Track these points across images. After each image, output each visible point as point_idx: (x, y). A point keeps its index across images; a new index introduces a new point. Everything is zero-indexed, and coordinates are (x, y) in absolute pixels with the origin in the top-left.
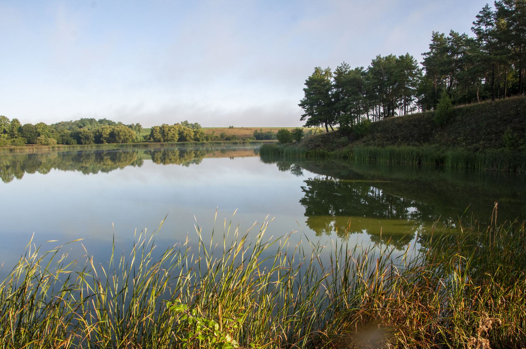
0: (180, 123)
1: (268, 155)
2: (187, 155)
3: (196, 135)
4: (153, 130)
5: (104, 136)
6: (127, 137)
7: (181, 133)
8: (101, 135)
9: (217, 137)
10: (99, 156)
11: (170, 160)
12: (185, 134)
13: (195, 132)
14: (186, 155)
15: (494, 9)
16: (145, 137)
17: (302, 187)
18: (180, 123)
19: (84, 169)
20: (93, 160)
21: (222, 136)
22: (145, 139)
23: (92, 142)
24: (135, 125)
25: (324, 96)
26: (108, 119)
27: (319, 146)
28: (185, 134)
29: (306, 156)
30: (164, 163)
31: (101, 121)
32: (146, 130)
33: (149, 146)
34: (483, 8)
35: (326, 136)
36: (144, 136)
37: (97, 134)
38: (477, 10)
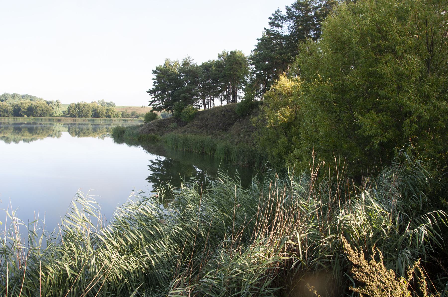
0: (97, 101)
1: (120, 136)
2: (100, 130)
3: (107, 112)
4: (70, 107)
5: (23, 110)
6: (45, 112)
7: (94, 110)
8: (19, 109)
9: (128, 115)
10: (18, 129)
11: (84, 133)
12: (98, 111)
13: (107, 110)
14: (98, 130)
15: (284, 13)
16: (64, 112)
17: (149, 165)
18: (97, 101)
19: (5, 138)
20: (12, 131)
21: (133, 114)
22: (64, 114)
23: (11, 114)
24: (55, 101)
25: (174, 84)
26: (30, 94)
27: (153, 130)
28: (98, 111)
29: (140, 139)
30: (79, 136)
31: (23, 97)
32: (64, 105)
33: (62, 121)
34: (275, 11)
35: (162, 121)
36: (63, 112)
37: (16, 107)
38: (270, 13)
